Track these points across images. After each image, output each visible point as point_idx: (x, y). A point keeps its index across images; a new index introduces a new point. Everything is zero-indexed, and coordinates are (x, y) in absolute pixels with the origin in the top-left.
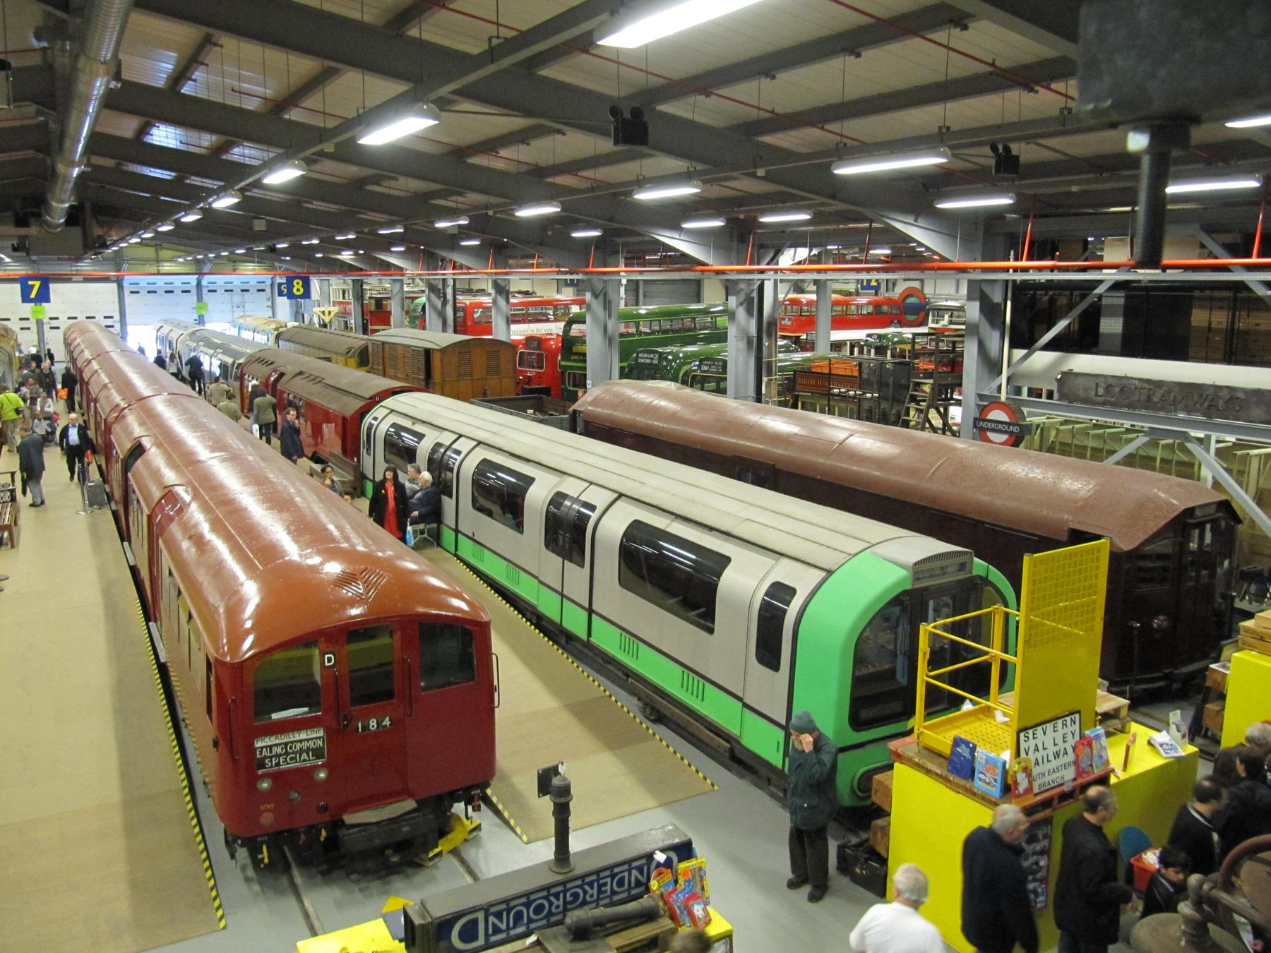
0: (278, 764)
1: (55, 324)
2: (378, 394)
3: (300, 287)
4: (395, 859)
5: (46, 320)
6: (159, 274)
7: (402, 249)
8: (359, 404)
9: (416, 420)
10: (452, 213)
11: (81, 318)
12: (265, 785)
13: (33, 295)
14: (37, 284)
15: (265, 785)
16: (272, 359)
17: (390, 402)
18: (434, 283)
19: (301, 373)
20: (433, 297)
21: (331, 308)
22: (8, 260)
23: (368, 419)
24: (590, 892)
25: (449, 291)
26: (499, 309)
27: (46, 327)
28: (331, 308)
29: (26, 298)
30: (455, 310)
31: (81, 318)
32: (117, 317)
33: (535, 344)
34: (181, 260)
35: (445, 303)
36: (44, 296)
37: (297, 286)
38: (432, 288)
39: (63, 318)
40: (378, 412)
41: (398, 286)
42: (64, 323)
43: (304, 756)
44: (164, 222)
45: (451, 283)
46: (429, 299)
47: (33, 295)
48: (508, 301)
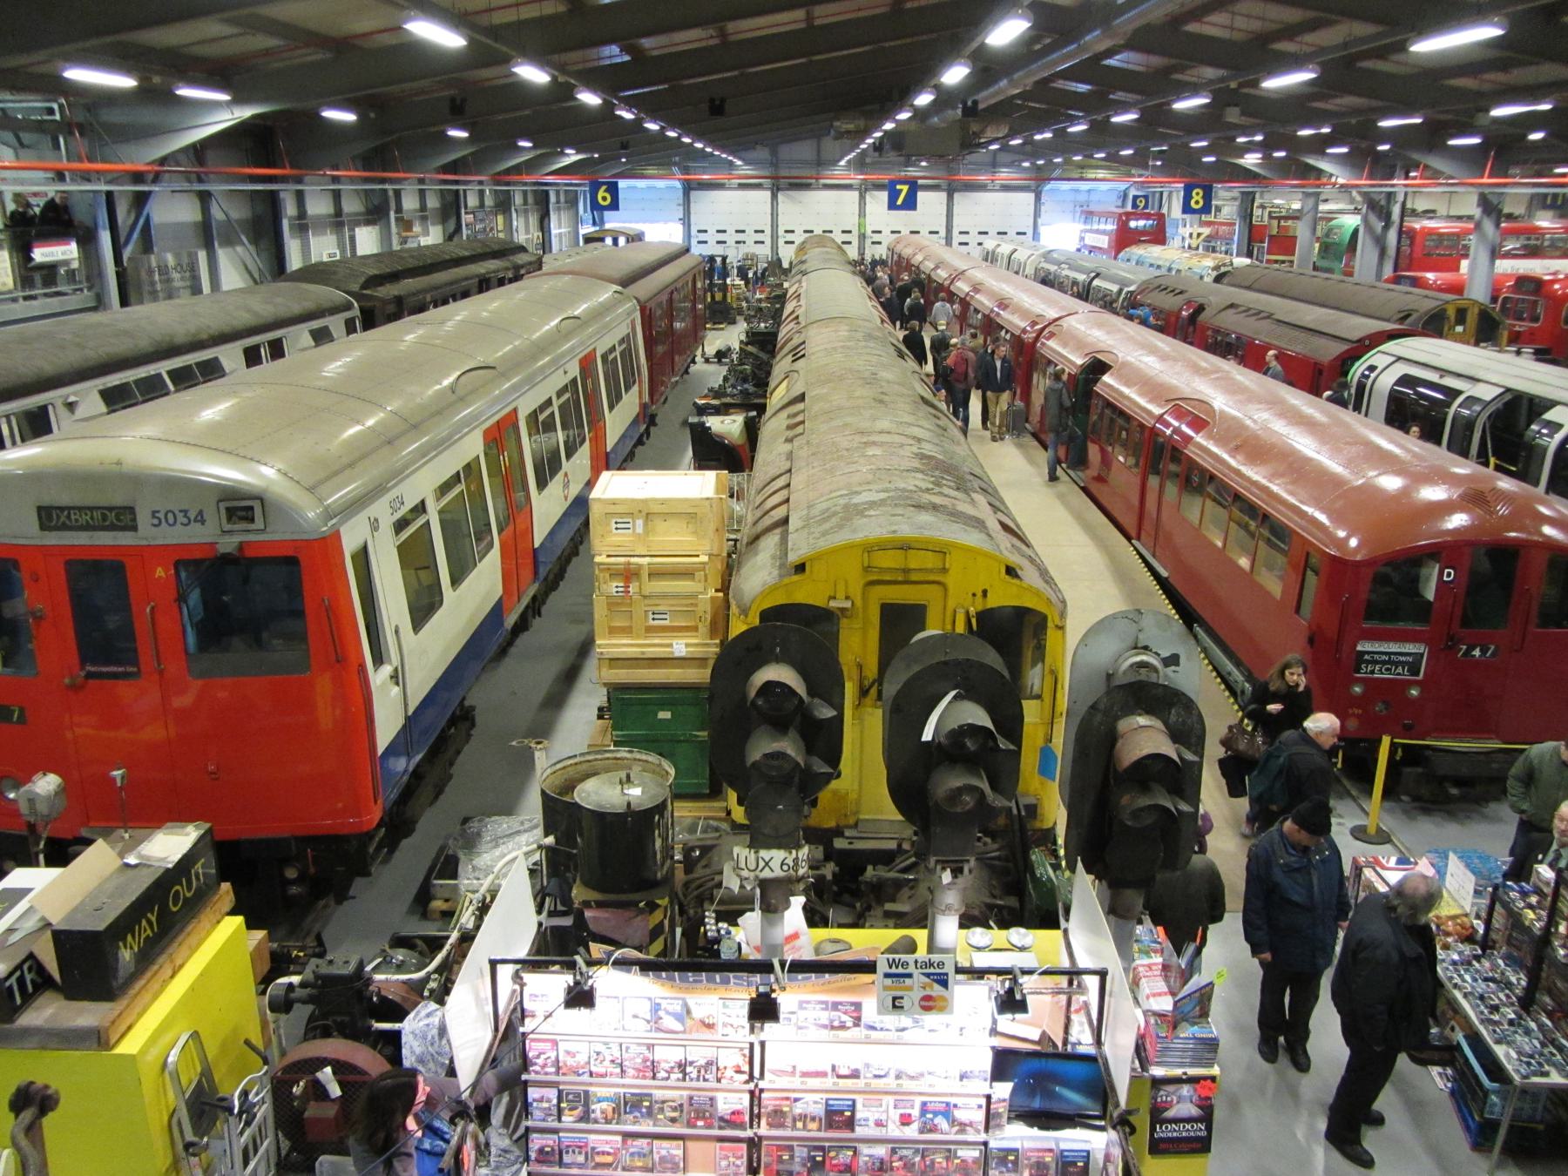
0: (1372, 672)
1: (789, 237)
2: (1370, 337)
3: (1199, 198)
4: (1454, 791)
5: (869, 233)
6: (1082, 179)
7: (1344, 150)
8: (1338, 349)
9: (1444, 372)
10: (1194, 89)
11: (905, 232)
12: (1357, 689)
13: (899, 202)
14: (905, 188)
15: (1357, 689)
16: (1181, 287)
17: (1390, 346)
18: (1377, 198)
19: (1232, 306)
20: (1373, 219)
21: (1200, 230)
22: (739, 163)
23: (1358, 369)
25: (1396, 210)
26: (1483, 236)
27: (868, 242)
28: (1200, 230)
29: (892, 206)
30: (1400, 232)
31: (905, 232)
32: (781, 242)
33: (1532, 286)
34: (1026, 164)
35: (1386, 227)
36: (910, 204)
37: (1196, 198)
38: (1372, 205)
39: (886, 231)
40: (1377, 358)
41: (1311, 202)
42: (799, 238)
43: (1400, 670)
44: (900, 110)
45: (1400, 198)
46: (1365, 220)
47: (899, 202)
48: (1497, 225)
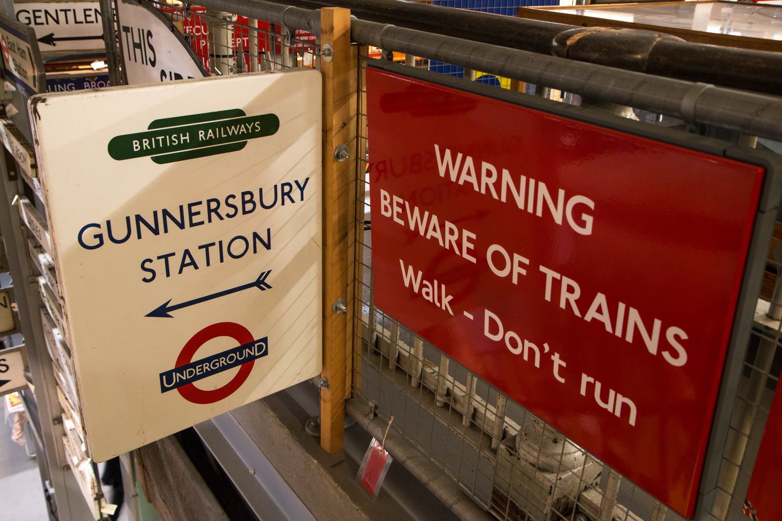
3: (138, 145)
24: (207, 368)
